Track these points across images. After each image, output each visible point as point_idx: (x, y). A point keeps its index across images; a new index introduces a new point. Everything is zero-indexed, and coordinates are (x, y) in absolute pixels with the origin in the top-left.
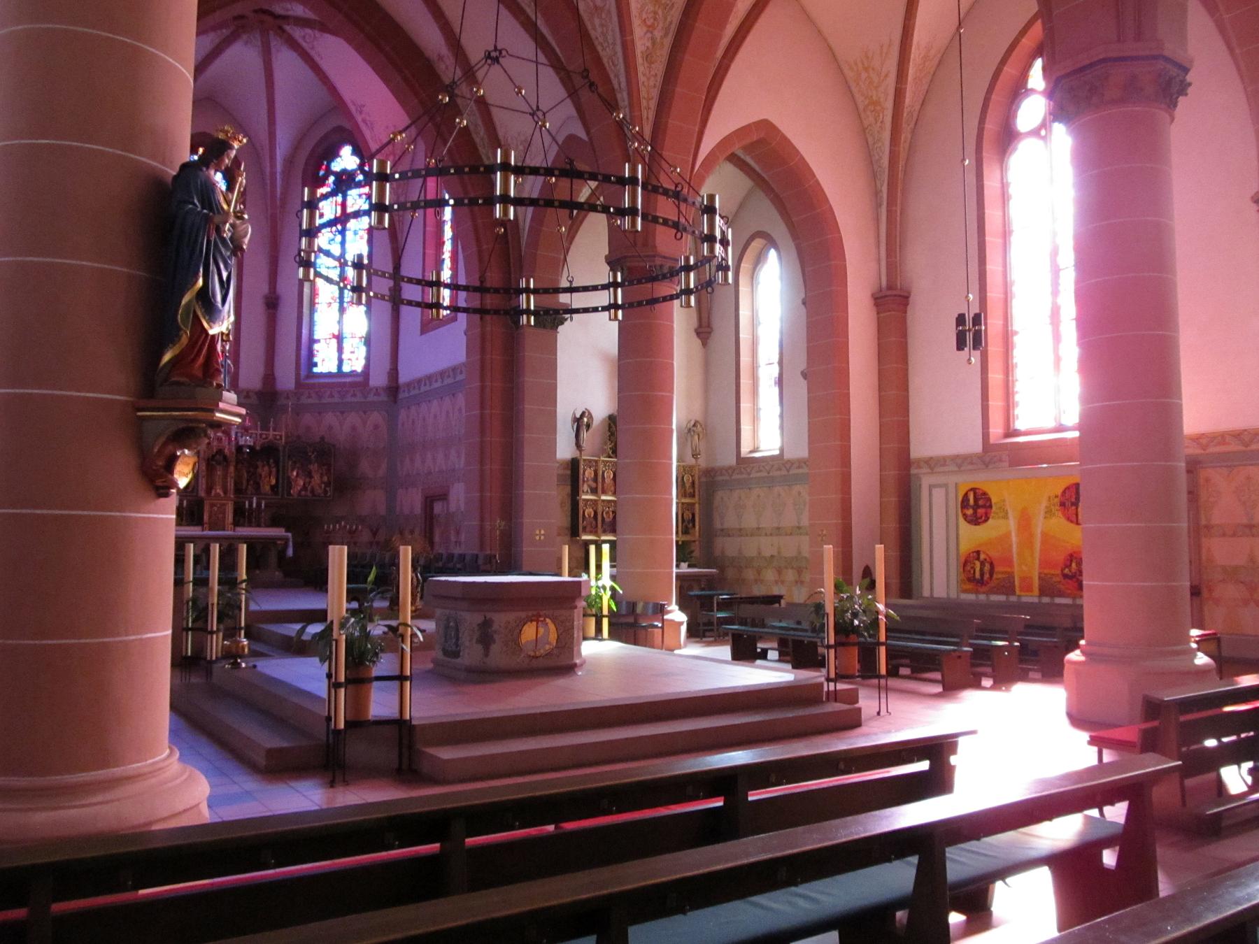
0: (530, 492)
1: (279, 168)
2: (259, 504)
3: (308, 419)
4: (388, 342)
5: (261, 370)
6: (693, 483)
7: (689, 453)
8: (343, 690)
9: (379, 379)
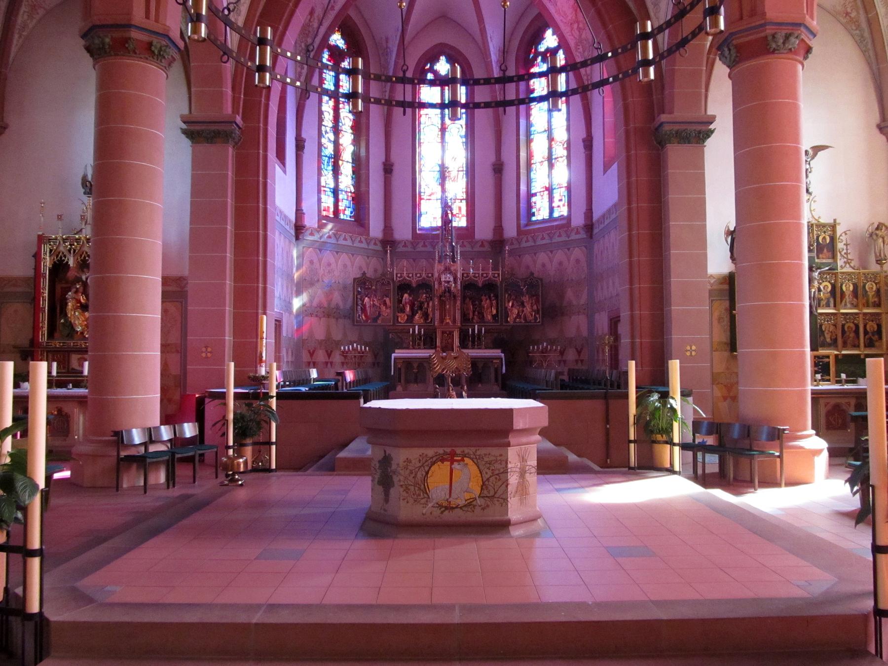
0: (677, 308)
2: (480, 331)
3: (527, 259)
4: (585, 188)
5: (381, 226)
7: (872, 259)
9: (578, 221)
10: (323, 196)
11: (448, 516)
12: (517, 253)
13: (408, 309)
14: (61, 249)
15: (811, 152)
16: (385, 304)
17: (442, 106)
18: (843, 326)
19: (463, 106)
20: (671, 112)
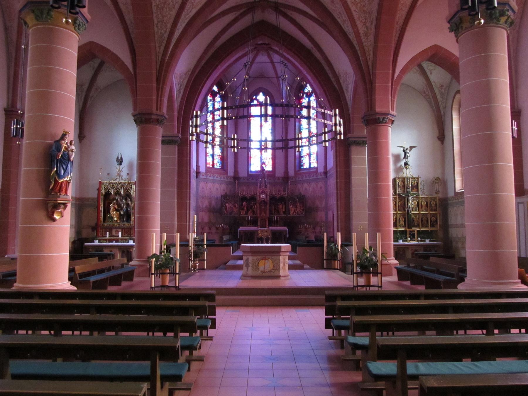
0: (355, 211)
3: (299, 186)
4: (323, 156)
5: (233, 170)
6: (436, 205)
8: (153, 276)
9: (321, 170)
10: (208, 158)
11: (264, 274)
13: (245, 209)
14: (109, 187)
15: (409, 148)
16: (235, 206)
17: (261, 116)
18: (422, 219)
19: (270, 116)
20: (353, 133)
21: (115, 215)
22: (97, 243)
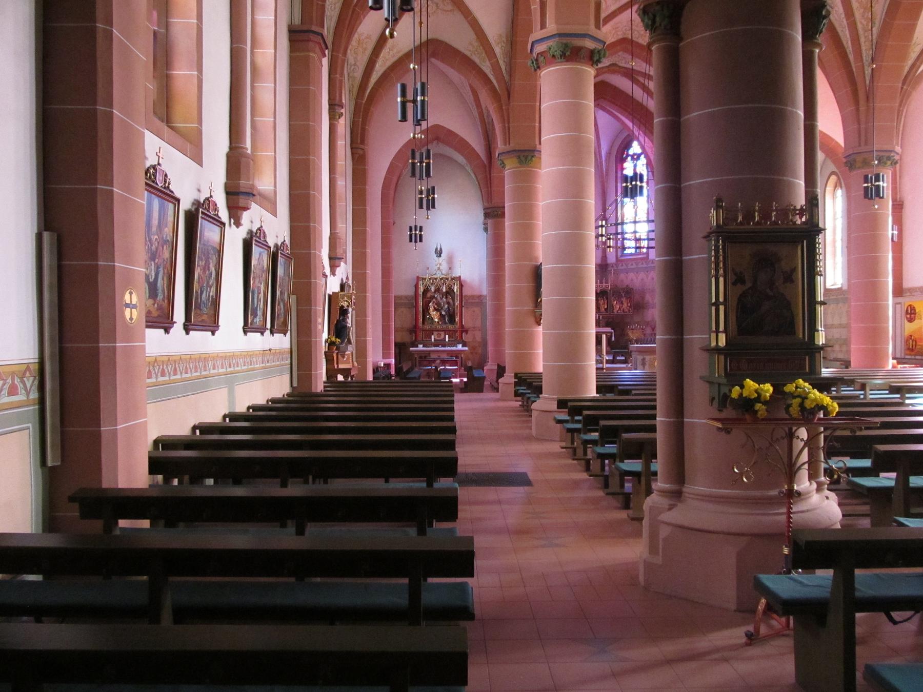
1: (604, 159)
3: (622, 276)
12: (617, 273)
21: (435, 316)
22: (421, 347)
